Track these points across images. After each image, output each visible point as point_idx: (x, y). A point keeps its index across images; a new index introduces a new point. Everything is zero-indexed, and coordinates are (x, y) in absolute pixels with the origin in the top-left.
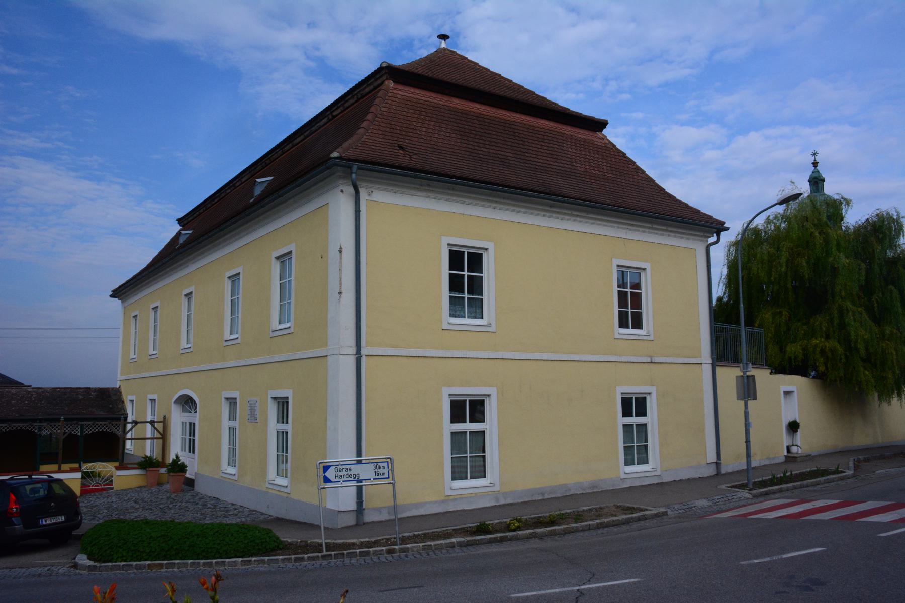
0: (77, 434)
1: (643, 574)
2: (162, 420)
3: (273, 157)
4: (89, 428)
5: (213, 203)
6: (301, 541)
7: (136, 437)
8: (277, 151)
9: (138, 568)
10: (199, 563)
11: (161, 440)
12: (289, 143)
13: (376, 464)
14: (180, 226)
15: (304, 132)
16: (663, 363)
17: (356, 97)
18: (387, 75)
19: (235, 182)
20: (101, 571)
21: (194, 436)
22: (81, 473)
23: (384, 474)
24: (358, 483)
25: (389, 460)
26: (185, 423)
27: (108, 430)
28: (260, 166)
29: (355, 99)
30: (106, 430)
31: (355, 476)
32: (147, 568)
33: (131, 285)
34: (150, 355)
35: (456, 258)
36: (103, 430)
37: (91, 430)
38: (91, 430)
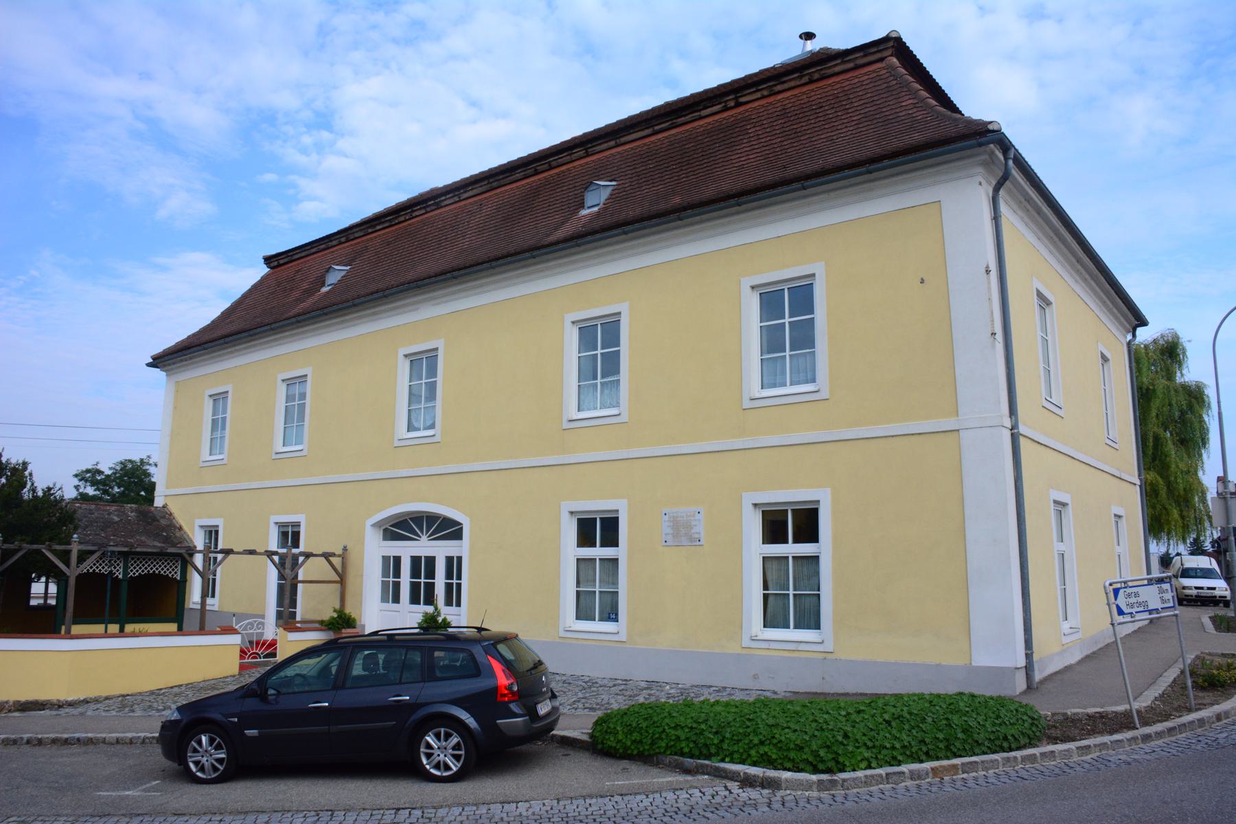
0: (117, 576)
1: (728, 735)
3: (559, 160)
5: (370, 230)
6: (1053, 715)
9: (914, 776)
10: (1015, 758)
12: (612, 140)
18: (894, 49)
19: (590, 145)
20: (848, 789)
24: (1150, 614)
27: (162, 572)
29: (805, 79)
30: (160, 572)
32: (931, 775)
34: (277, 453)
36: (154, 571)
37: (137, 571)
38: (137, 571)
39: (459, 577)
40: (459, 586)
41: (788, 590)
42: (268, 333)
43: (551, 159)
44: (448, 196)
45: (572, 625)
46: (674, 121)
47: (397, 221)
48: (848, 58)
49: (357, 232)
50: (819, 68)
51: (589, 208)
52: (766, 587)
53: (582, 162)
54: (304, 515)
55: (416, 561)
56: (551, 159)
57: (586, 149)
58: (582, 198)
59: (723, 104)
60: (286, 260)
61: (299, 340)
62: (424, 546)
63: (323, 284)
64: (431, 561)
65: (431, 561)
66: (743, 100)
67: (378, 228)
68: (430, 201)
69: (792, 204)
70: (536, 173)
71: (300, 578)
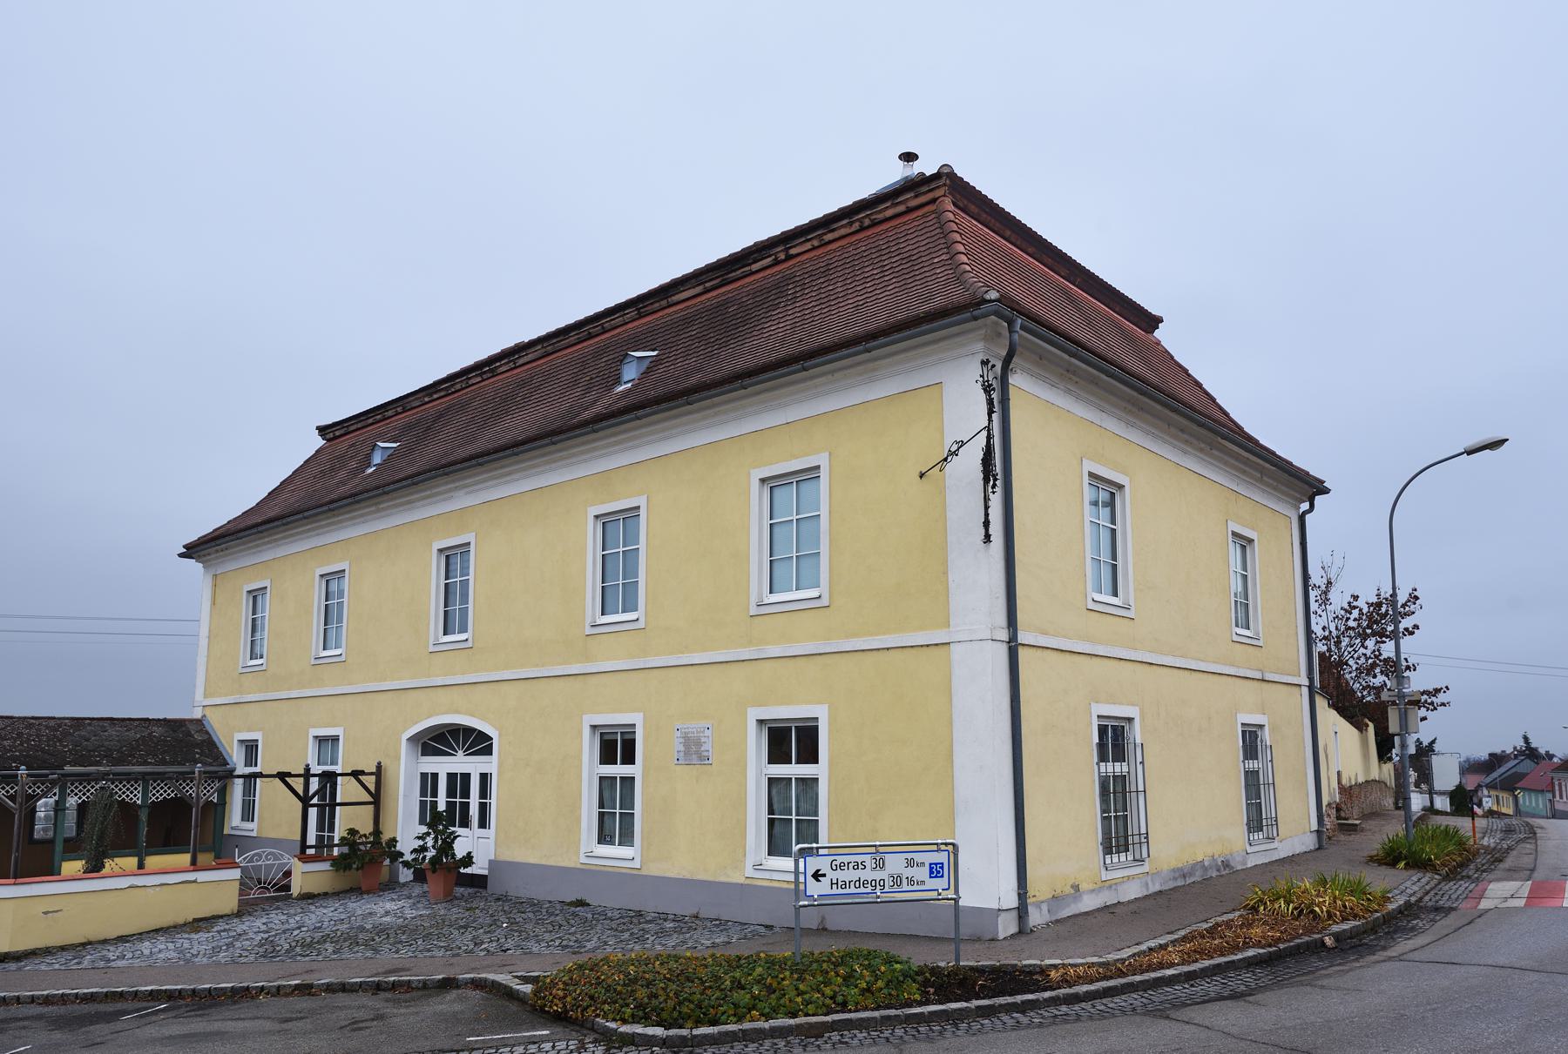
2: (302, 772)
4: (158, 791)
5: (426, 399)
7: (343, 801)
11: (371, 807)
15: (706, 282)
16: (1250, 678)
19: (498, 364)
22: (239, 870)
26: (435, 776)
29: (856, 226)
31: (873, 883)
33: (238, 539)
37: (161, 795)
39: (254, 796)
40: (254, 800)
41: (791, 815)
42: (301, 522)
43: (604, 321)
44: (503, 362)
45: (764, 862)
46: (726, 277)
47: (453, 390)
48: (899, 200)
49: (413, 400)
50: (868, 213)
51: (625, 383)
52: (771, 811)
53: (636, 323)
54: (749, 709)
55: (451, 777)
56: (604, 321)
57: (638, 309)
58: (618, 372)
59: (774, 257)
60: (342, 432)
61: (585, 461)
62: (460, 763)
63: (618, 381)
64: (466, 777)
65: (466, 777)
66: (793, 251)
67: (435, 396)
68: (486, 366)
69: (917, 352)
70: (591, 337)
71: (338, 801)
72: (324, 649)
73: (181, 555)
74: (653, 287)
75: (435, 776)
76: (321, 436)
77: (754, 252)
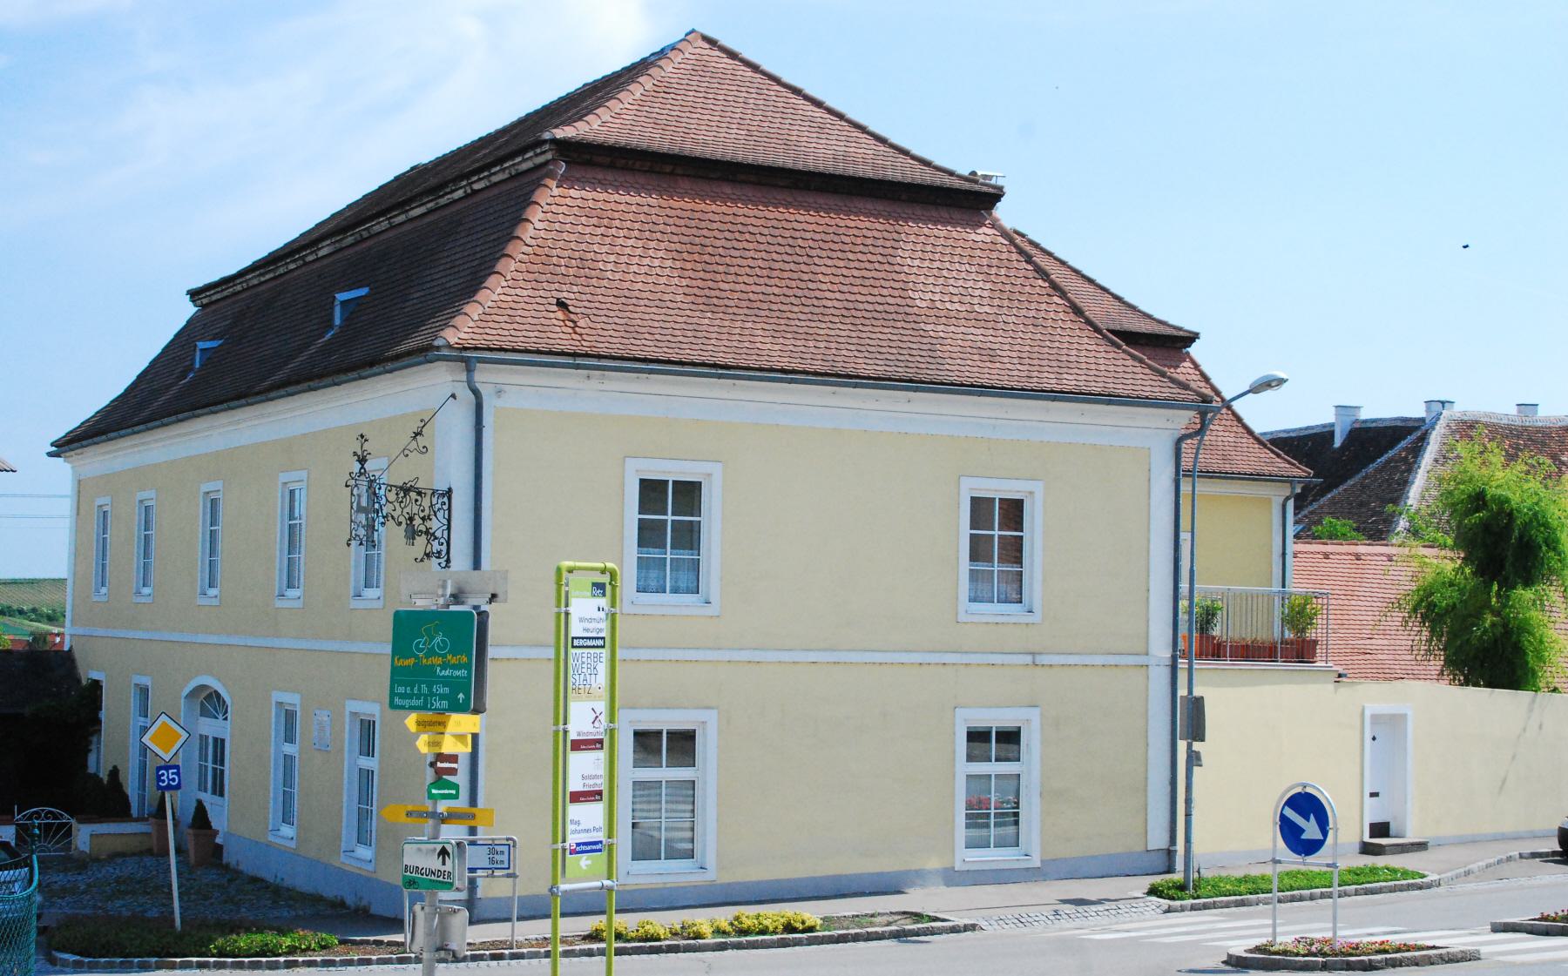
8: (381, 219)
13: (491, 847)
14: (196, 306)
17: (507, 171)
21: (222, 764)
23: (502, 862)
25: (511, 842)
26: (207, 737)
28: (350, 239)
35: (651, 491)
72: (144, 586)
73: (50, 454)
74: (248, 265)
75: (207, 737)
76: (193, 301)
77: (304, 248)
